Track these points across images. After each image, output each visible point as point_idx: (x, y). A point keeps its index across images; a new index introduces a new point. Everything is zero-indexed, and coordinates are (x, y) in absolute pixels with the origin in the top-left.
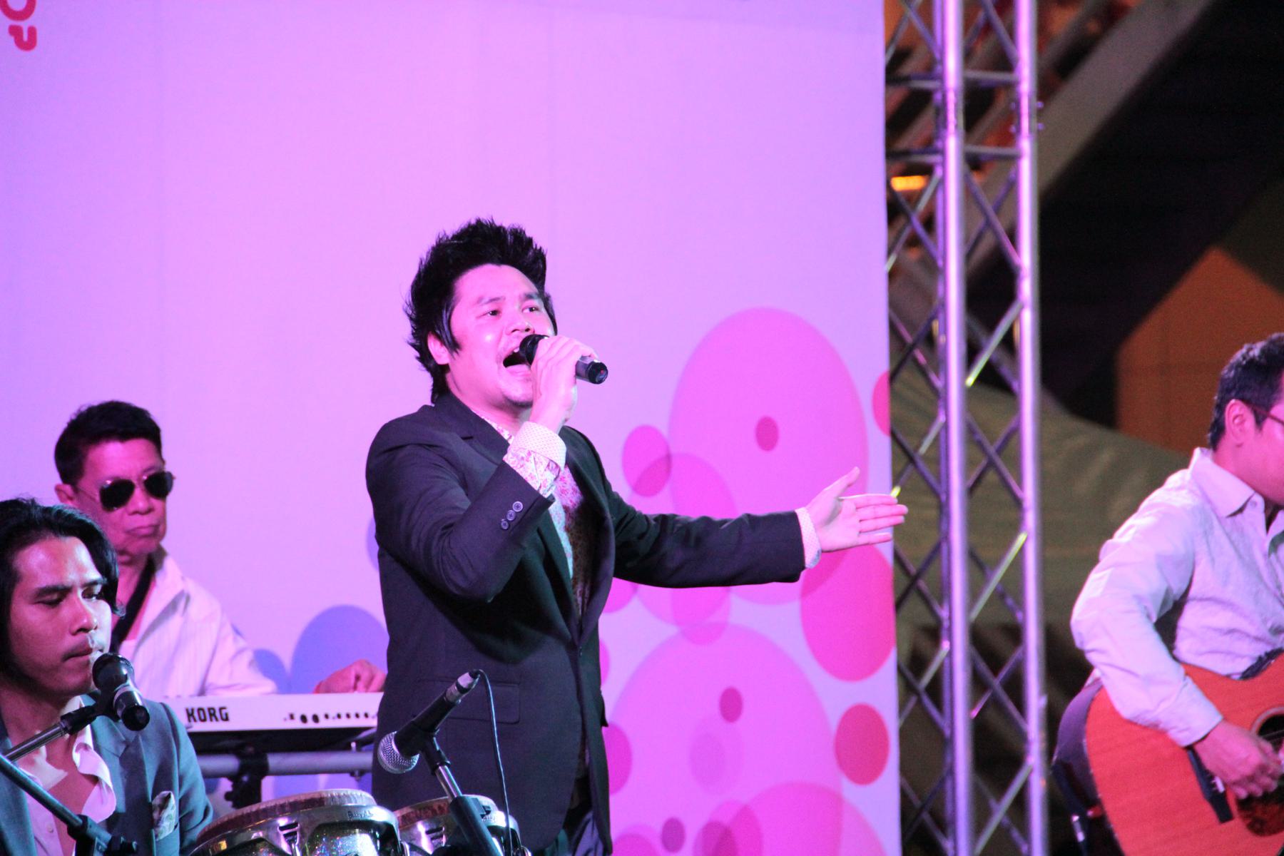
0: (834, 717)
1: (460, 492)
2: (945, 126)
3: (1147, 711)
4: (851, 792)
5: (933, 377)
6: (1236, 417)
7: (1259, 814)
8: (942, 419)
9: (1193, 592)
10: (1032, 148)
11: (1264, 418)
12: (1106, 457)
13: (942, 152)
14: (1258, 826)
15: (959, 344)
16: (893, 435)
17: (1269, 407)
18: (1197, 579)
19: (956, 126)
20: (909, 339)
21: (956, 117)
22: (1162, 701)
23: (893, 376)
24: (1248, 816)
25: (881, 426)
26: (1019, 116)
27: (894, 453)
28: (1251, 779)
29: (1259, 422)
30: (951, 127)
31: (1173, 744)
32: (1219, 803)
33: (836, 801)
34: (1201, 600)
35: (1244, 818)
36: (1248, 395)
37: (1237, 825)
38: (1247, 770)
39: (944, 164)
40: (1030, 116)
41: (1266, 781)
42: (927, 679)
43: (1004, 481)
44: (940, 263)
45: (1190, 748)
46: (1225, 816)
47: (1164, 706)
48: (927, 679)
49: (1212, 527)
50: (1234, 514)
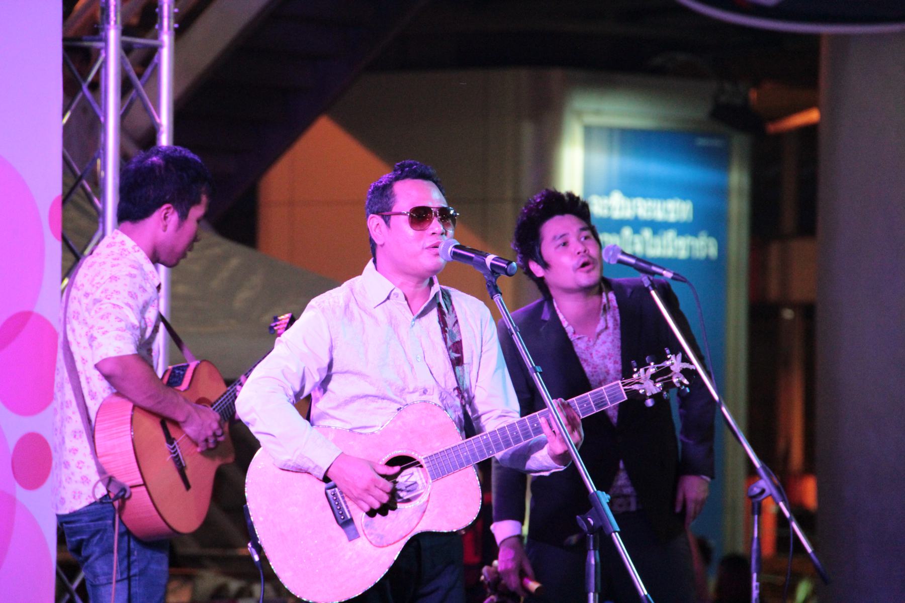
0: (12, 443)
2: (108, 23)
3: (289, 460)
4: (22, 494)
5: (96, 200)
8: (103, 55)
10: (169, 41)
11: (389, 216)
12: (234, 262)
13: (106, 40)
15: (114, 178)
16: (65, 240)
17: (390, 209)
19: (116, 22)
20: (79, 173)
21: (116, 16)
23: (66, 198)
25: (56, 236)
26: (162, 18)
27: (63, 250)
30: (112, 23)
33: (12, 501)
39: (106, 48)
40: (169, 18)
42: (76, 583)
43: (146, 109)
44: (102, 119)
48: (76, 583)
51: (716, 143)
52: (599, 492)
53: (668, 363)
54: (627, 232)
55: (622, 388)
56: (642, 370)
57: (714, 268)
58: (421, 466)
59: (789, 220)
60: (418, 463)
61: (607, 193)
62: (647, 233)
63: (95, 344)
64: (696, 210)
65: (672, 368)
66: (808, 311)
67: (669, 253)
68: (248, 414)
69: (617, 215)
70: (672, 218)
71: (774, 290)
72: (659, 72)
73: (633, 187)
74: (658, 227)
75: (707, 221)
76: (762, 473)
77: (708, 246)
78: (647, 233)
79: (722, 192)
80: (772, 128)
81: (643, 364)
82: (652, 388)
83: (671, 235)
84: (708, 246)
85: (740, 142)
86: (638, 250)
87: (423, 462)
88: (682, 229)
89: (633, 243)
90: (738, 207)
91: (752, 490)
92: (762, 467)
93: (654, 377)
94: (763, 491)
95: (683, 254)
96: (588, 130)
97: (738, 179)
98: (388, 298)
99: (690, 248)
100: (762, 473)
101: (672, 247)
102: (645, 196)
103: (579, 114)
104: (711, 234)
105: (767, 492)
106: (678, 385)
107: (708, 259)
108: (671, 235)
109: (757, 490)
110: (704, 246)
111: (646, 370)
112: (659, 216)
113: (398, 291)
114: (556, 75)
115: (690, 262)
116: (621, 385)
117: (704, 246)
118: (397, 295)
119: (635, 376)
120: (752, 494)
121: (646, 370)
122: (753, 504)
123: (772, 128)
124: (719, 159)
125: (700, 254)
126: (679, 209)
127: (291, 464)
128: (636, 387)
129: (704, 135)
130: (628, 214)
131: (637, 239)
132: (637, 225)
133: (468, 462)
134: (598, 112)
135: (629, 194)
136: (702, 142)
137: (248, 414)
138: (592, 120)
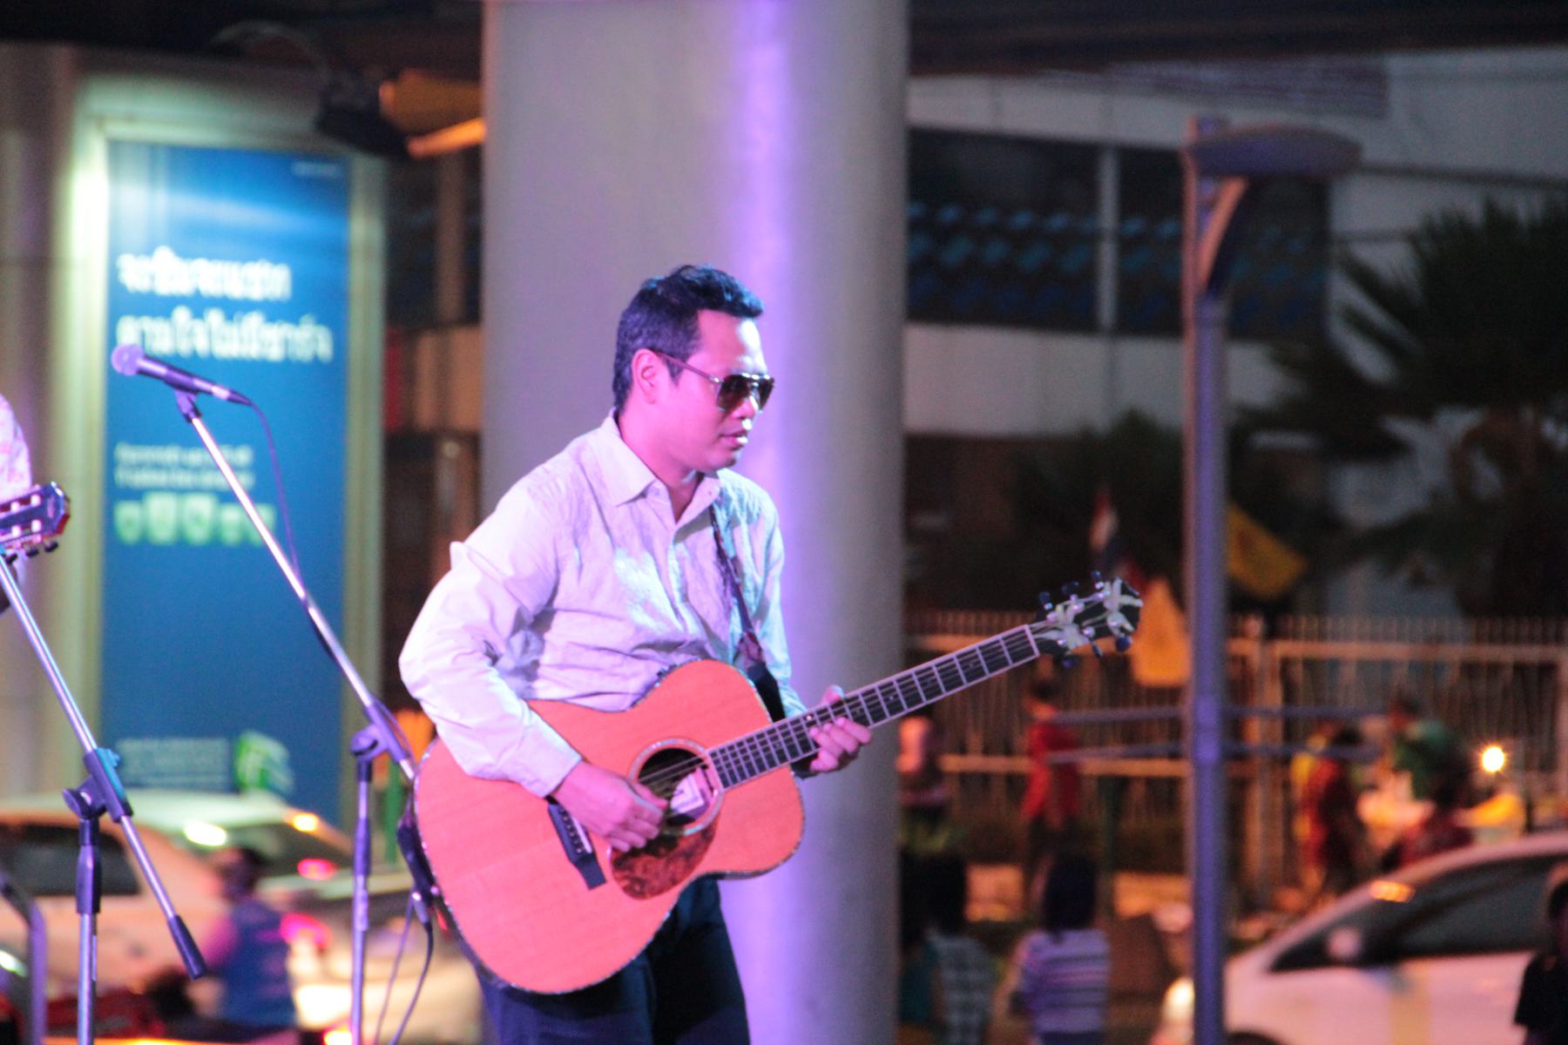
1: (804, 794)
3: (490, 765)
6: (644, 370)
7: (639, 873)
9: (558, 603)
11: (680, 370)
14: (637, 888)
17: (684, 358)
18: (562, 589)
22: (505, 750)
24: (626, 877)
28: (625, 826)
29: (675, 375)
31: (535, 796)
32: (585, 862)
34: (566, 610)
35: (618, 880)
36: (660, 344)
37: (612, 888)
38: (618, 815)
41: (646, 826)
45: (550, 799)
46: (594, 878)
47: (506, 756)
49: (586, 525)
50: (635, 499)
51: (327, 170)
52: (101, 751)
53: (1101, 595)
54: (182, 314)
55: (1031, 638)
56: (1059, 608)
57: (325, 377)
58: (705, 767)
59: (449, 297)
60: (700, 760)
61: (149, 251)
62: (215, 317)
63: (531, 605)
64: (297, 282)
65: (1107, 605)
66: (473, 442)
67: (252, 351)
68: (418, 685)
69: (164, 288)
70: (256, 294)
71: (425, 414)
72: (230, 52)
73: (193, 241)
74: (233, 308)
75: (316, 298)
76: (374, 714)
77: (315, 340)
78: (215, 317)
79: (338, 252)
80: (419, 147)
81: (1059, 598)
82: (1073, 640)
83: (254, 320)
84: (315, 340)
85: (365, 169)
86: (201, 346)
87: (709, 761)
88: (274, 311)
89: (191, 334)
90: (365, 278)
91: (357, 742)
92: (376, 706)
93: (1079, 619)
94: (374, 744)
95: (275, 353)
96: (116, 148)
97: (364, 230)
98: (643, 495)
99: (286, 343)
100: (374, 714)
101: (260, 340)
102: (211, 257)
103: (100, 121)
104: (321, 321)
105: (382, 745)
106: (1116, 632)
107: (316, 360)
108: (254, 320)
109: (364, 743)
110: (309, 340)
111: (1066, 608)
112: (236, 291)
113: (659, 486)
114: (60, 56)
115: (288, 367)
116: (1028, 632)
117: (309, 340)
118: (657, 493)
119: (1050, 616)
120: (357, 748)
121: (1066, 608)
122: (359, 766)
123: (419, 147)
124: (333, 197)
125: (303, 352)
126: (270, 279)
127: (493, 770)
128: (1052, 635)
129: (309, 157)
130: (183, 287)
131: (199, 327)
132: (199, 304)
133: (783, 759)
134: (130, 118)
135: (185, 252)
136: (303, 169)
137: (418, 685)
138: (121, 130)
